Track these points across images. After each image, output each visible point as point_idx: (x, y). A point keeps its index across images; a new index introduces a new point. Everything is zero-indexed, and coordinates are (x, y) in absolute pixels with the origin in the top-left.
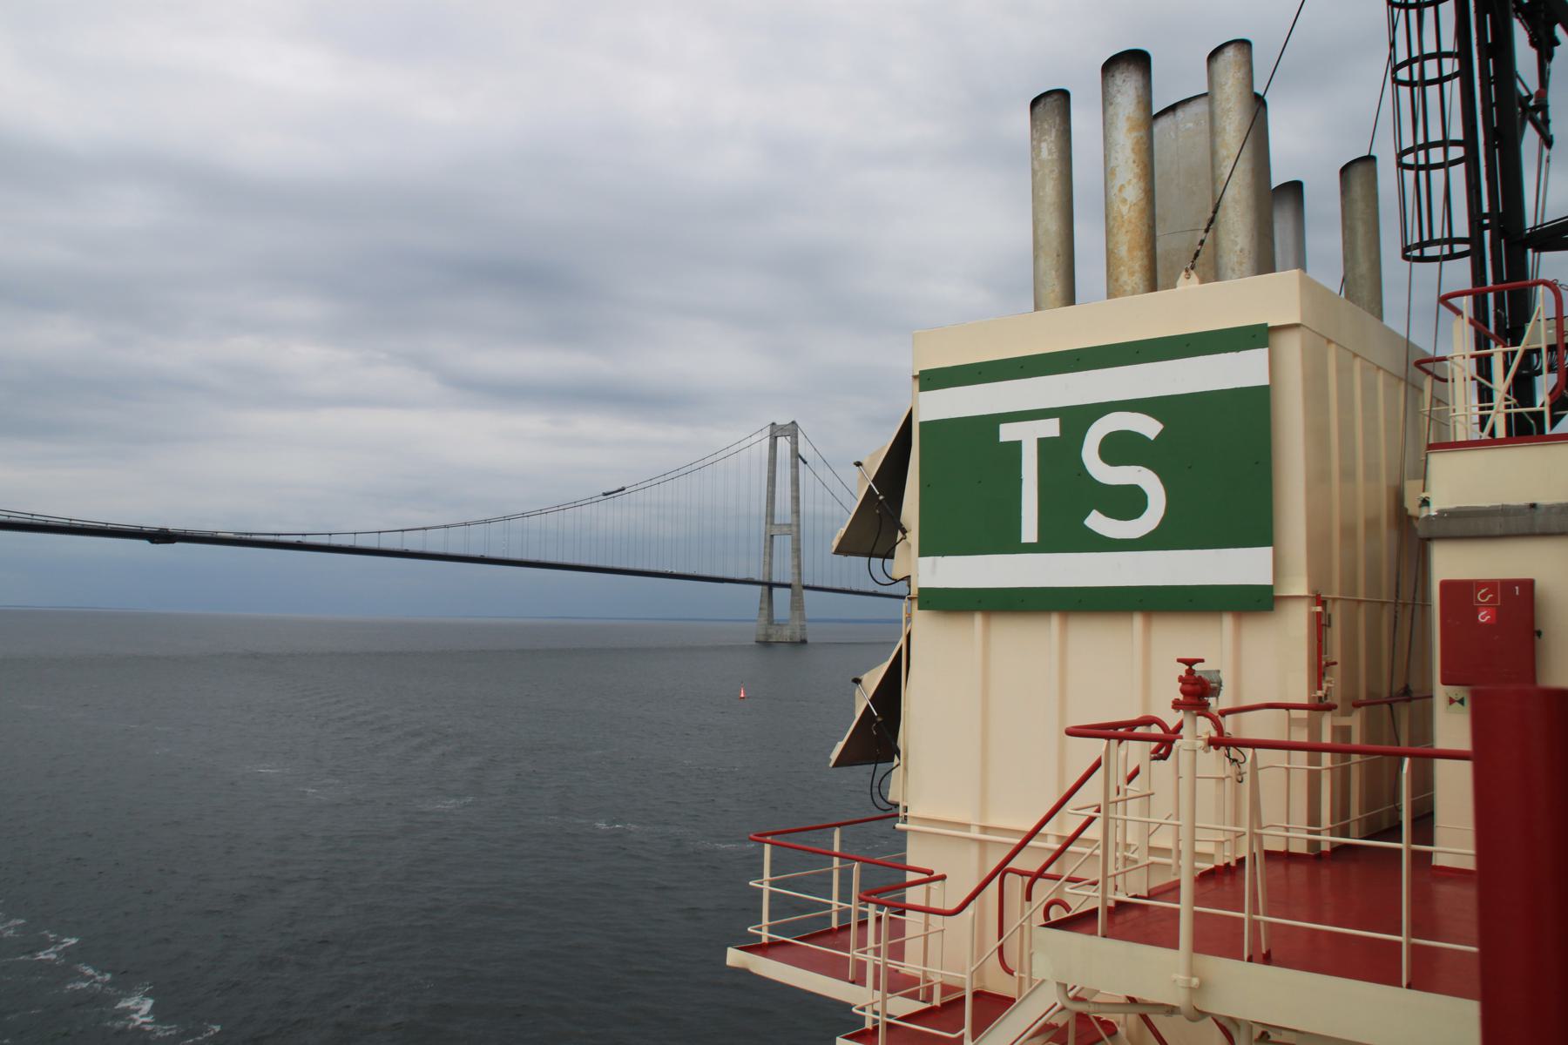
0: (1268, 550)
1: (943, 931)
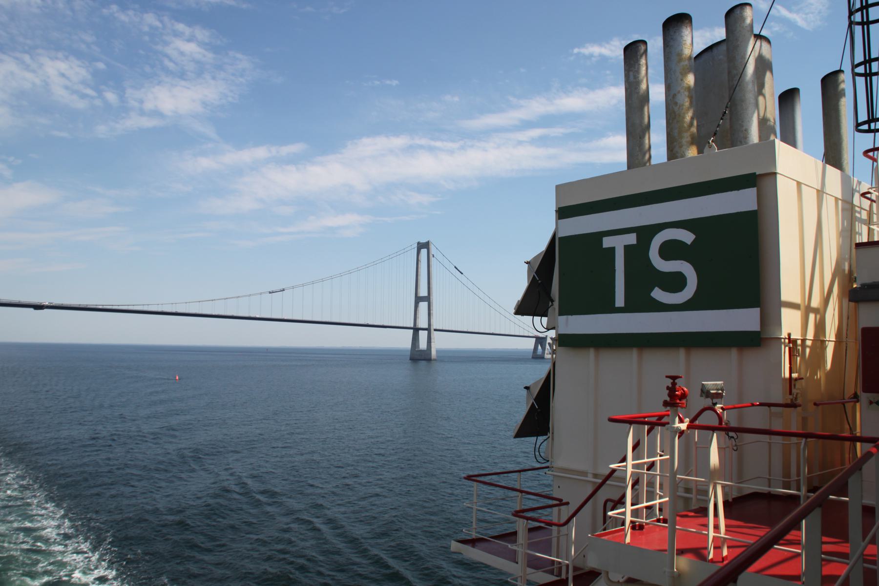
0: (758, 310)
1: (567, 535)
